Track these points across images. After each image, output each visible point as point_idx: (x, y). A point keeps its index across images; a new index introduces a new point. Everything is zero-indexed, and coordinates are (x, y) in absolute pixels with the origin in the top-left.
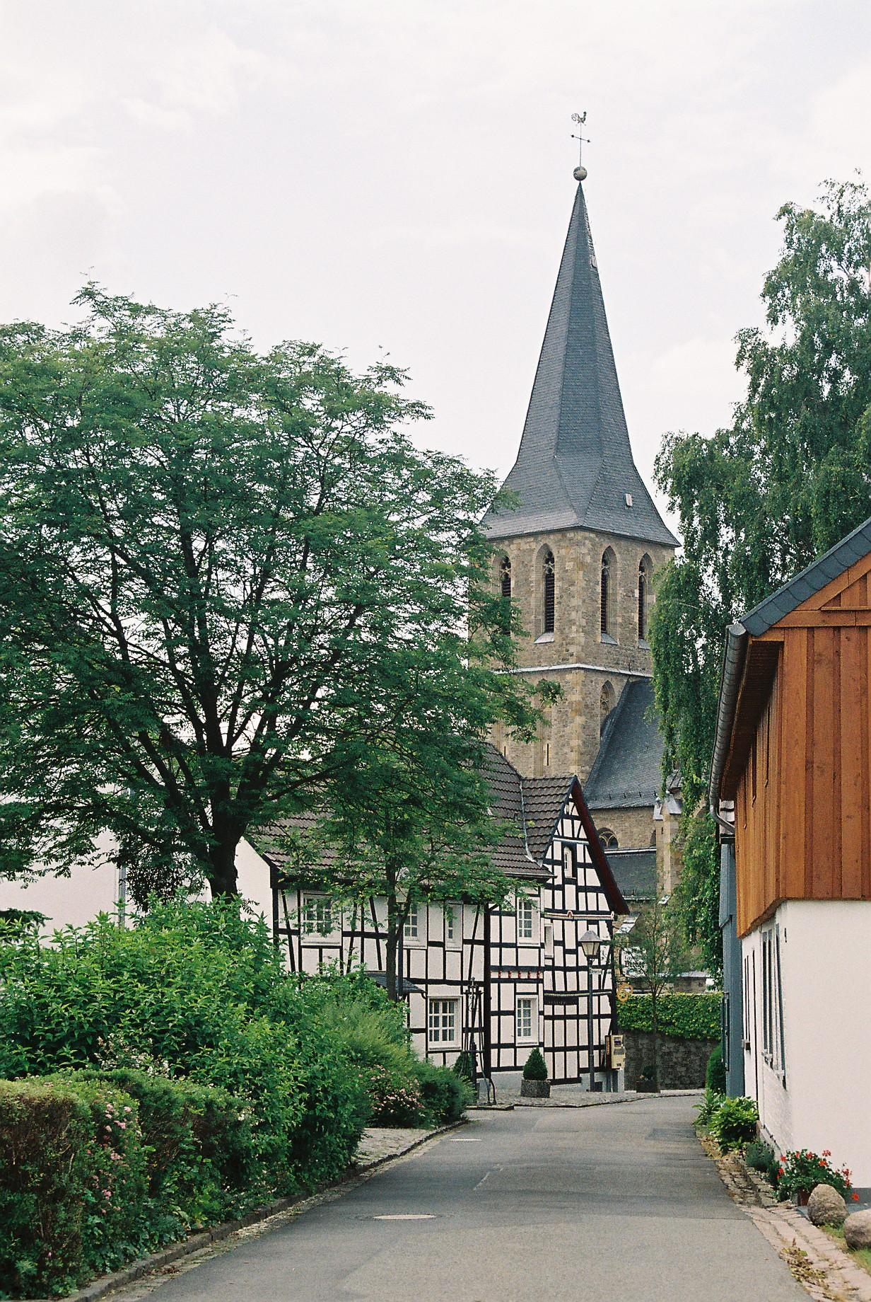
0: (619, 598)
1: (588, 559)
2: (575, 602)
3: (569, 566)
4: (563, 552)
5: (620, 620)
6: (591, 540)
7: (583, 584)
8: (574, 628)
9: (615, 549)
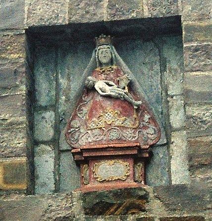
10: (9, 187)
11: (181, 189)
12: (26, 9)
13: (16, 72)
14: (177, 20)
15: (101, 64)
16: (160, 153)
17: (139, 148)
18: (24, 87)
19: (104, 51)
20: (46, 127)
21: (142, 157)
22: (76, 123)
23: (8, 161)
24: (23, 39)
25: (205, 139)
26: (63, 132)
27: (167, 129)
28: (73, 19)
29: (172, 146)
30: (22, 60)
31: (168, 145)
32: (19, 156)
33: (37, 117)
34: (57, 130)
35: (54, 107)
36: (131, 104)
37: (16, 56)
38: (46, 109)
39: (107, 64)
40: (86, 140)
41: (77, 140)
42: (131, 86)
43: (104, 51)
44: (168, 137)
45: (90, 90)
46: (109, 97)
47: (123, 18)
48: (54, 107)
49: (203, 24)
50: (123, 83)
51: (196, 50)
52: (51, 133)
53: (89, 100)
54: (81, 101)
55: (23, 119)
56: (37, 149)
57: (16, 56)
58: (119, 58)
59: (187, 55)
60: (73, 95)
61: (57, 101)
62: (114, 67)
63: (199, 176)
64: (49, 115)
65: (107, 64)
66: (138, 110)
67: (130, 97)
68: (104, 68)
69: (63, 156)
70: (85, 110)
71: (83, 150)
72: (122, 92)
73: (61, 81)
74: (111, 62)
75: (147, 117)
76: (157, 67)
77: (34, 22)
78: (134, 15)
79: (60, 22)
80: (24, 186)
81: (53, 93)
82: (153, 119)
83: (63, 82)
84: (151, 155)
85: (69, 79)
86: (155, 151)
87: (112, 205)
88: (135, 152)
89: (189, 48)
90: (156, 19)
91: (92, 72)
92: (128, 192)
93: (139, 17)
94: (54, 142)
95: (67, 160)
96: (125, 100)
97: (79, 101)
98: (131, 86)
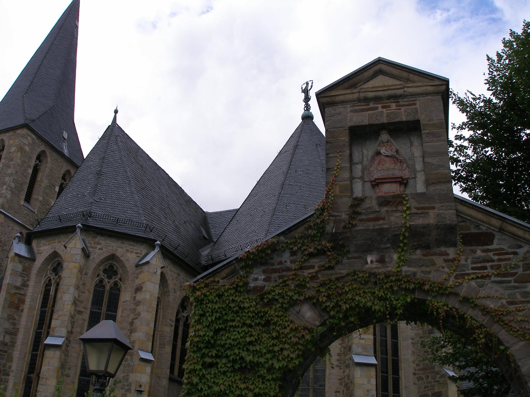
0: (43, 185)
1: (27, 148)
2: (10, 171)
3: (13, 149)
4: (11, 142)
5: (41, 198)
6: (32, 139)
7: (19, 162)
8: (5, 187)
9: (48, 154)
10: (342, 194)
11: (422, 194)
12: (348, 118)
13: (344, 145)
14: (418, 121)
15: (383, 142)
16: (411, 182)
17: (402, 177)
18: (348, 152)
19: (384, 136)
20: (358, 170)
21: (403, 182)
22: (372, 169)
23: (341, 183)
24: (348, 131)
25: (434, 172)
26: (366, 173)
27: (415, 171)
28: (370, 122)
29: (417, 179)
30: (347, 140)
31: (415, 178)
32: (346, 181)
33: (353, 167)
34: (363, 172)
35: (361, 163)
36: (397, 159)
37: (344, 138)
38: (357, 163)
39: (386, 142)
40: (377, 175)
41: (372, 176)
42: (397, 151)
43: (384, 136)
44: (415, 175)
45: (378, 153)
46: (387, 156)
47: (393, 121)
48: (361, 163)
49: (431, 123)
50: (394, 150)
51: (428, 134)
52: (360, 174)
53: (378, 158)
54: (374, 159)
55: (348, 165)
56: (354, 181)
57: (344, 138)
58: (392, 140)
59: (423, 136)
60: (369, 157)
61: (362, 160)
62: (389, 144)
63: (432, 188)
64: (359, 167)
65: (386, 142)
66: (400, 162)
67: (397, 156)
68: (385, 144)
69: (366, 183)
70: (376, 162)
71: (376, 179)
72: (393, 153)
73: (364, 152)
74: (388, 141)
75: (405, 166)
76: (409, 145)
77: (352, 124)
78: (398, 120)
79: (364, 123)
80: (349, 194)
81: (361, 157)
82: (408, 166)
83: (365, 152)
84: (407, 182)
85: (368, 151)
86: (409, 181)
87: (390, 202)
88: (400, 180)
89: (425, 133)
90: (408, 121)
91: (379, 145)
92: (398, 196)
93: (401, 120)
94: (362, 178)
95: (368, 185)
96: (395, 157)
97: (373, 158)
98: (397, 151)
